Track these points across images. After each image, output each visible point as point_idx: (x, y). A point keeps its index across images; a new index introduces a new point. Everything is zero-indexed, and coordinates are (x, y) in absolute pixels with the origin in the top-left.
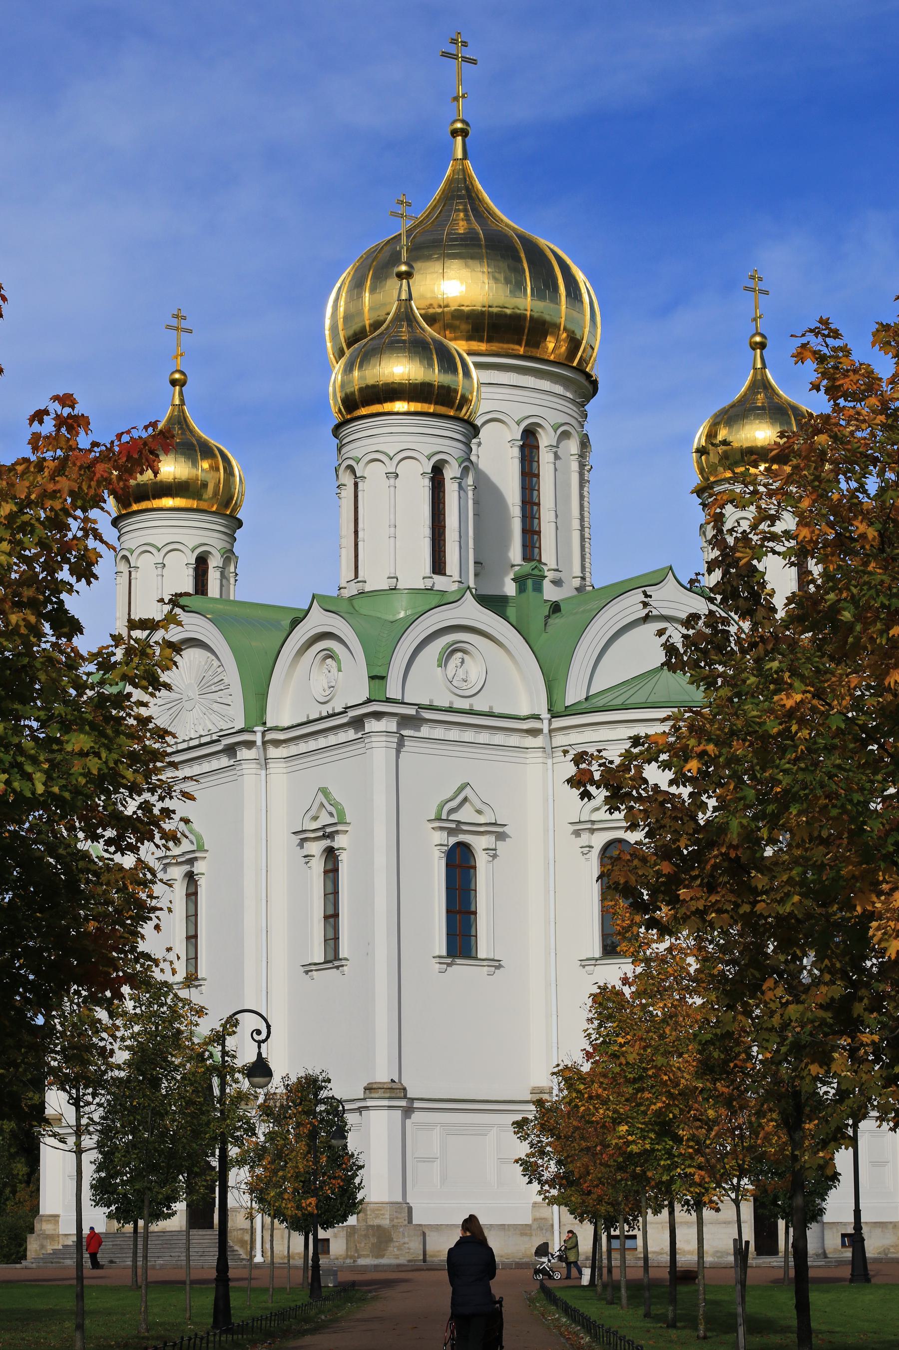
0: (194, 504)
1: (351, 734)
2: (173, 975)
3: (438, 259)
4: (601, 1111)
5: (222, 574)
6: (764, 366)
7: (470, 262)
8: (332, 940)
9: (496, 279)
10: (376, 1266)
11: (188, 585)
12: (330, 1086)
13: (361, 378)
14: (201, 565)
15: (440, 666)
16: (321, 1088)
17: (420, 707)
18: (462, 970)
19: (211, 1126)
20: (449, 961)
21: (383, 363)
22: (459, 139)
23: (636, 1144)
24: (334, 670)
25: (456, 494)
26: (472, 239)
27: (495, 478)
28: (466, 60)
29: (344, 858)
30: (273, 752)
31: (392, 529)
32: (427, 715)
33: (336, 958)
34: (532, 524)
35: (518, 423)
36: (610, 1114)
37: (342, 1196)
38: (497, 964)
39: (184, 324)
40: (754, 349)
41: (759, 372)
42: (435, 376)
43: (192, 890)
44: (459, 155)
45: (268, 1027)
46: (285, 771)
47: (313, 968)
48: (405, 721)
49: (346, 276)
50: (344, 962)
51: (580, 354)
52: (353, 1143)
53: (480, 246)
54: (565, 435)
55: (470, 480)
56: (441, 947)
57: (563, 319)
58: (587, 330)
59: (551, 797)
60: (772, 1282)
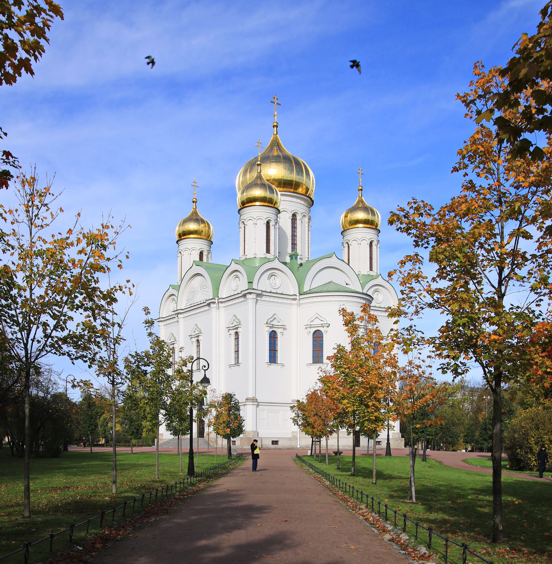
0: (199, 237)
1: (242, 299)
2: (131, 295)
4: (337, 394)
6: (362, 196)
7: (278, 163)
8: (237, 358)
9: (285, 169)
11: (198, 259)
12: (235, 396)
13: (246, 195)
14: (201, 254)
16: (233, 397)
17: (262, 291)
18: (273, 366)
22: (275, 128)
26: (279, 157)
27: (284, 228)
30: (220, 305)
32: (264, 294)
33: (238, 363)
35: (291, 212)
36: (341, 395)
39: (196, 185)
42: (268, 195)
43: (198, 345)
45: (208, 364)
48: (258, 295)
49: (242, 170)
52: (242, 413)
54: (304, 216)
56: (267, 359)
58: (311, 185)
60: (362, 455)
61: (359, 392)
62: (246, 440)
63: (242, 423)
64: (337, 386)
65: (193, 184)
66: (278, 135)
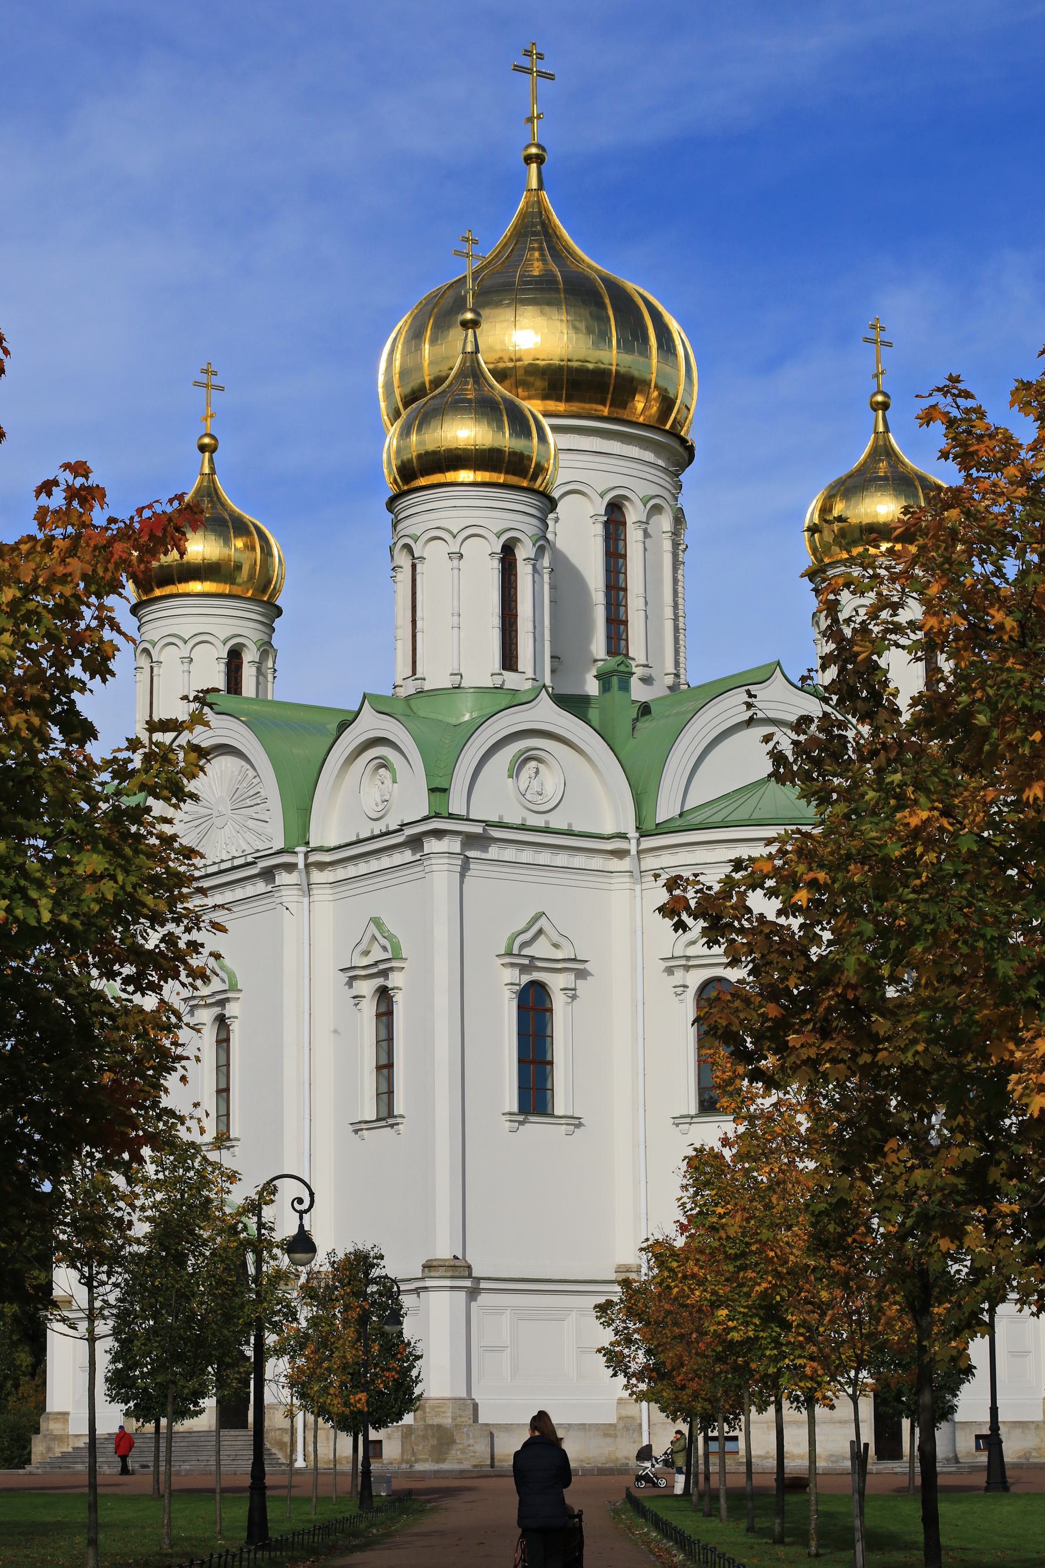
0: (226, 589)
1: (407, 856)
2: (202, 1134)
3: (509, 305)
4: (697, 1293)
5: (259, 669)
6: (887, 430)
7: (547, 308)
8: (386, 1094)
9: (576, 329)
10: (436, 1472)
12: (382, 1263)
13: (420, 443)
15: (511, 776)
16: (372, 1266)
17: (488, 824)
18: (536, 1129)
19: (246, 1310)
20: (521, 1118)
21: (445, 426)
22: (534, 166)
23: (738, 1331)
24: (388, 781)
25: (530, 578)
28: (541, 74)
29: (400, 1000)
30: (317, 876)
31: (456, 618)
33: (391, 1114)
34: (618, 612)
35: (602, 495)
36: (708, 1296)
37: (397, 1390)
38: (576, 1122)
40: (875, 410)
41: (881, 436)
42: (506, 440)
43: (223, 1036)
44: (534, 185)
45: (312, 1195)
46: (331, 898)
47: (364, 1126)
48: (470, 840)
49: (403, 323)
50: (399, 1120)
51: (673, 415)
52: (409, 1329)
53: (557, 290)
54: (657, 509)
55: (546, 562)
56: (511, 1101)
57: (654, 375)
58: (682, 388)
59: (639, 929)
61: (757, 1288)
62: (425, 1437)
63: (412, 1367)
64: (696, 1269)
65: (203, 379)
66: (544, 194)
